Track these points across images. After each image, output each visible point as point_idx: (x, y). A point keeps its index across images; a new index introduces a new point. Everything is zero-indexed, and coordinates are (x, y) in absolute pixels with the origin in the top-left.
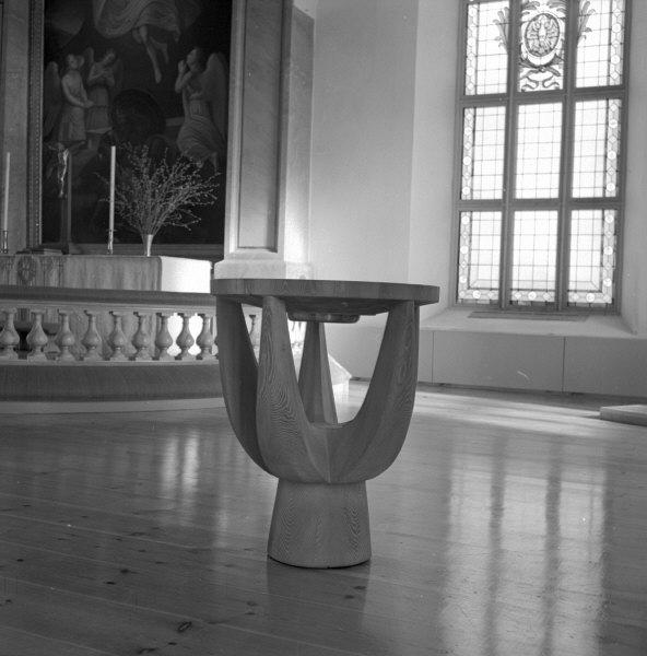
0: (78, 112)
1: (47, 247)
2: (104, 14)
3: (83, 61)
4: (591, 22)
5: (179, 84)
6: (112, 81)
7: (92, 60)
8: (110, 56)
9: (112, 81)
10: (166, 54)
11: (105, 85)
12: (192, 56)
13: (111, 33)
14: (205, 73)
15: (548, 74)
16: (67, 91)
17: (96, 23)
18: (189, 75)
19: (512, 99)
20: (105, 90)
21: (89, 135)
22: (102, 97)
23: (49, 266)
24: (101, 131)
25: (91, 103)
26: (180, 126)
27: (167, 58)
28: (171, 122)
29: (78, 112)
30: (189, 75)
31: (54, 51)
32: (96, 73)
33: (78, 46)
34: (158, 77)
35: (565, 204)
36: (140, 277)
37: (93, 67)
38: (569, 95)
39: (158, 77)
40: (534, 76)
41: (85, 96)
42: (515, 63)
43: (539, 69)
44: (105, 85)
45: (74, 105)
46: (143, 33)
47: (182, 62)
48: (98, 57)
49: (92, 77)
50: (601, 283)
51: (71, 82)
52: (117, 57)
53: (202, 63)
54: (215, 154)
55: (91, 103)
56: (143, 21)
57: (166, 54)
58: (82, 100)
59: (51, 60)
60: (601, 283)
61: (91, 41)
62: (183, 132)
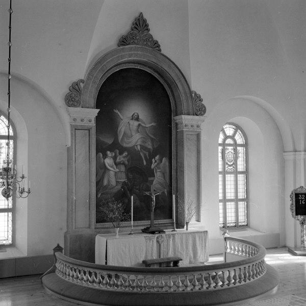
0: (112, 173)
1: (99, 233)
2: (122, 139)
3: (114, 154)
4: (240, 155)
5: (153, 166)
6: (126, 162)
7: (118, 155)
8: (125, 154)
9: (126, 162)
10: (148, 156)
11: (124, 164)
12: (157, 157)
13: (125, 145)
14: (162, 163)
15: (232, 167)
16: (107, 164)
17: (120, 141)
18: (156, 164)
19: (224, 173)
20: (123, 166)
21: (117, 182)
22: (123, 168)
23: (170, 237)
24: (123, 180)
25: (118, 170)
26: (153, 181)
27: (148, 158)
28: (150, 179)
29: (112, 173)
30: (156, 164)
31: (101, 149)
32: (120, 159)
33: (112, 148)
34: (145, 163)
35: (236, 200)
36: (201, 238)
37: (118, 157)
38: (236, 173)
39: (145, 163)
40: (229, 167)
41: (115, 166)
42: (224, 164)
43: (230, 166)
44: (124, 164)
45: (111, 170)
46: (139, 147)
47: (153, 159)
48: (121, 153)
49: (118, 160)
50: (8, 237)
51: (108, 162)
52: (128, 154)
53: (161, 160)
54: (166, 190)
55: (118, 170)
56: (139, 143)
57: (148, 156)
58: (114, 169)
59: (99, 152)
60: (8, 237)
61: (116, 147)
62: (154, 183)
